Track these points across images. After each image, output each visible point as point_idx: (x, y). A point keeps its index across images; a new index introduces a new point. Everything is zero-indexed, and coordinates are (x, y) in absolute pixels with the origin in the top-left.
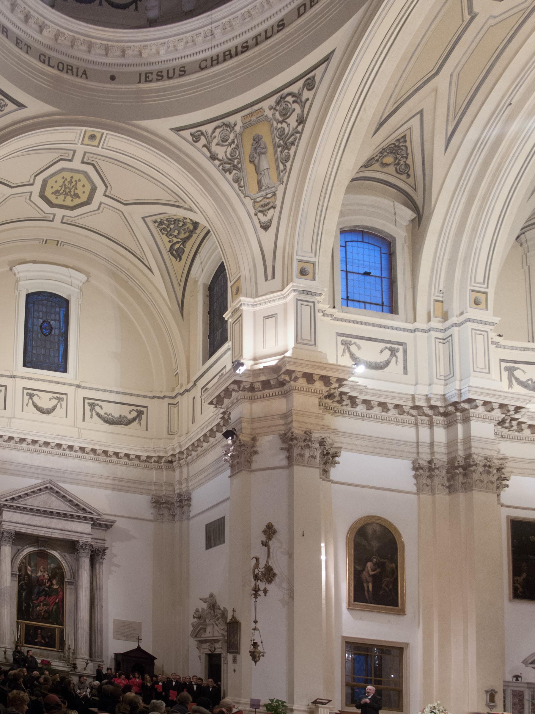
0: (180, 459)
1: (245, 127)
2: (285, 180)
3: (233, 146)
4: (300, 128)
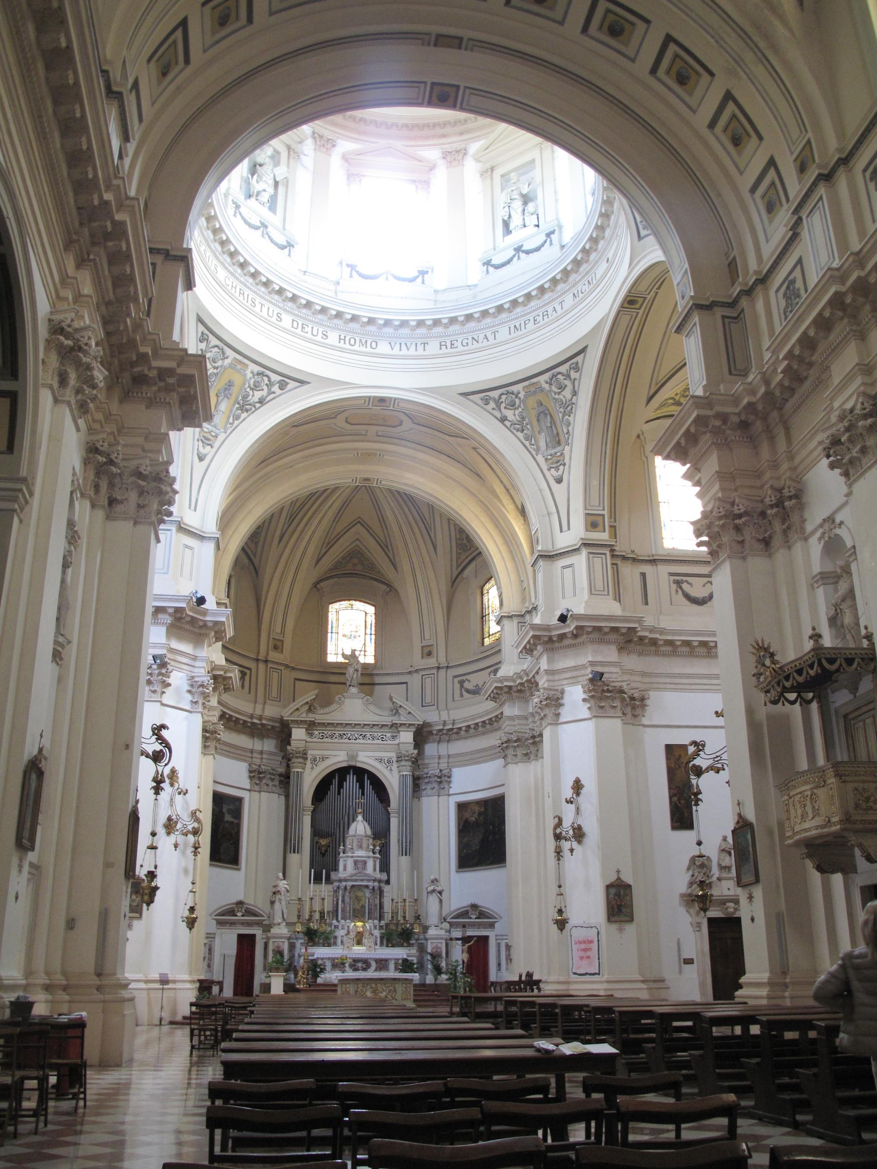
1: (231, 366)
2: (229, 431)
3: (215, 371)
4: (258, 405)
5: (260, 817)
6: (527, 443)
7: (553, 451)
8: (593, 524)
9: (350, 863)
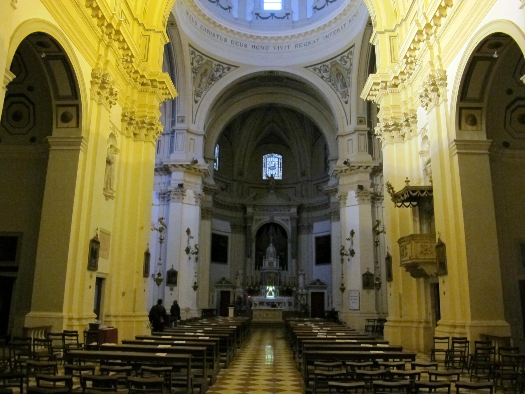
0: (403, 80)
5: (235, 245)
6: (333, 87)
7: (343, 90)
8: (360, 122)
9: (267, 263)
